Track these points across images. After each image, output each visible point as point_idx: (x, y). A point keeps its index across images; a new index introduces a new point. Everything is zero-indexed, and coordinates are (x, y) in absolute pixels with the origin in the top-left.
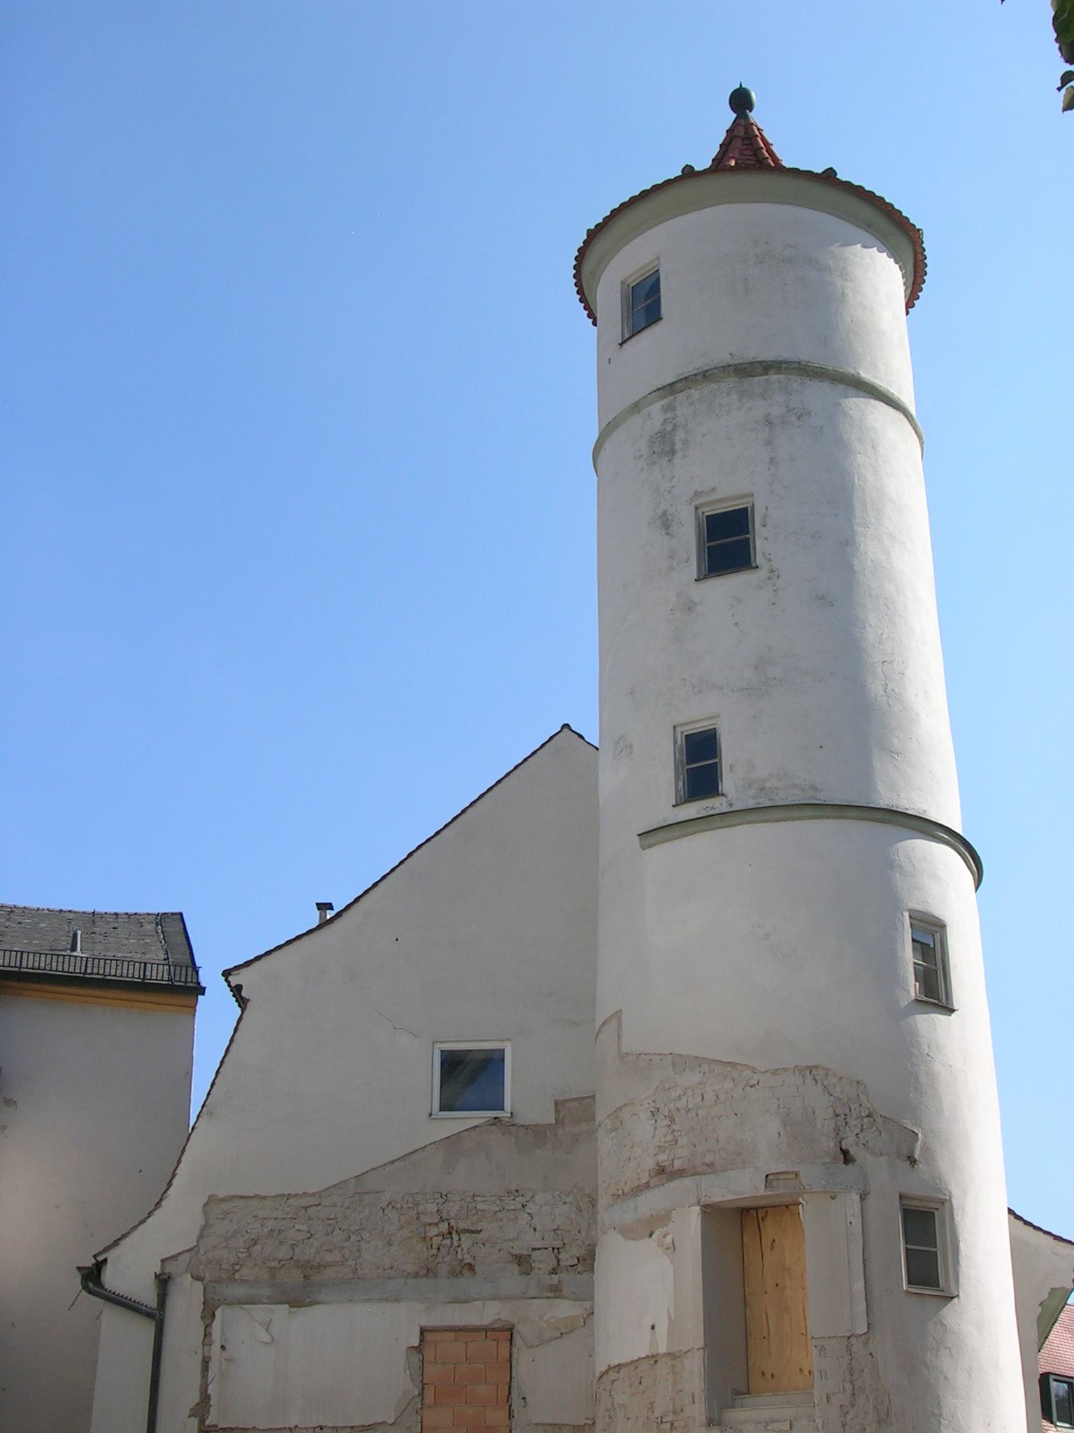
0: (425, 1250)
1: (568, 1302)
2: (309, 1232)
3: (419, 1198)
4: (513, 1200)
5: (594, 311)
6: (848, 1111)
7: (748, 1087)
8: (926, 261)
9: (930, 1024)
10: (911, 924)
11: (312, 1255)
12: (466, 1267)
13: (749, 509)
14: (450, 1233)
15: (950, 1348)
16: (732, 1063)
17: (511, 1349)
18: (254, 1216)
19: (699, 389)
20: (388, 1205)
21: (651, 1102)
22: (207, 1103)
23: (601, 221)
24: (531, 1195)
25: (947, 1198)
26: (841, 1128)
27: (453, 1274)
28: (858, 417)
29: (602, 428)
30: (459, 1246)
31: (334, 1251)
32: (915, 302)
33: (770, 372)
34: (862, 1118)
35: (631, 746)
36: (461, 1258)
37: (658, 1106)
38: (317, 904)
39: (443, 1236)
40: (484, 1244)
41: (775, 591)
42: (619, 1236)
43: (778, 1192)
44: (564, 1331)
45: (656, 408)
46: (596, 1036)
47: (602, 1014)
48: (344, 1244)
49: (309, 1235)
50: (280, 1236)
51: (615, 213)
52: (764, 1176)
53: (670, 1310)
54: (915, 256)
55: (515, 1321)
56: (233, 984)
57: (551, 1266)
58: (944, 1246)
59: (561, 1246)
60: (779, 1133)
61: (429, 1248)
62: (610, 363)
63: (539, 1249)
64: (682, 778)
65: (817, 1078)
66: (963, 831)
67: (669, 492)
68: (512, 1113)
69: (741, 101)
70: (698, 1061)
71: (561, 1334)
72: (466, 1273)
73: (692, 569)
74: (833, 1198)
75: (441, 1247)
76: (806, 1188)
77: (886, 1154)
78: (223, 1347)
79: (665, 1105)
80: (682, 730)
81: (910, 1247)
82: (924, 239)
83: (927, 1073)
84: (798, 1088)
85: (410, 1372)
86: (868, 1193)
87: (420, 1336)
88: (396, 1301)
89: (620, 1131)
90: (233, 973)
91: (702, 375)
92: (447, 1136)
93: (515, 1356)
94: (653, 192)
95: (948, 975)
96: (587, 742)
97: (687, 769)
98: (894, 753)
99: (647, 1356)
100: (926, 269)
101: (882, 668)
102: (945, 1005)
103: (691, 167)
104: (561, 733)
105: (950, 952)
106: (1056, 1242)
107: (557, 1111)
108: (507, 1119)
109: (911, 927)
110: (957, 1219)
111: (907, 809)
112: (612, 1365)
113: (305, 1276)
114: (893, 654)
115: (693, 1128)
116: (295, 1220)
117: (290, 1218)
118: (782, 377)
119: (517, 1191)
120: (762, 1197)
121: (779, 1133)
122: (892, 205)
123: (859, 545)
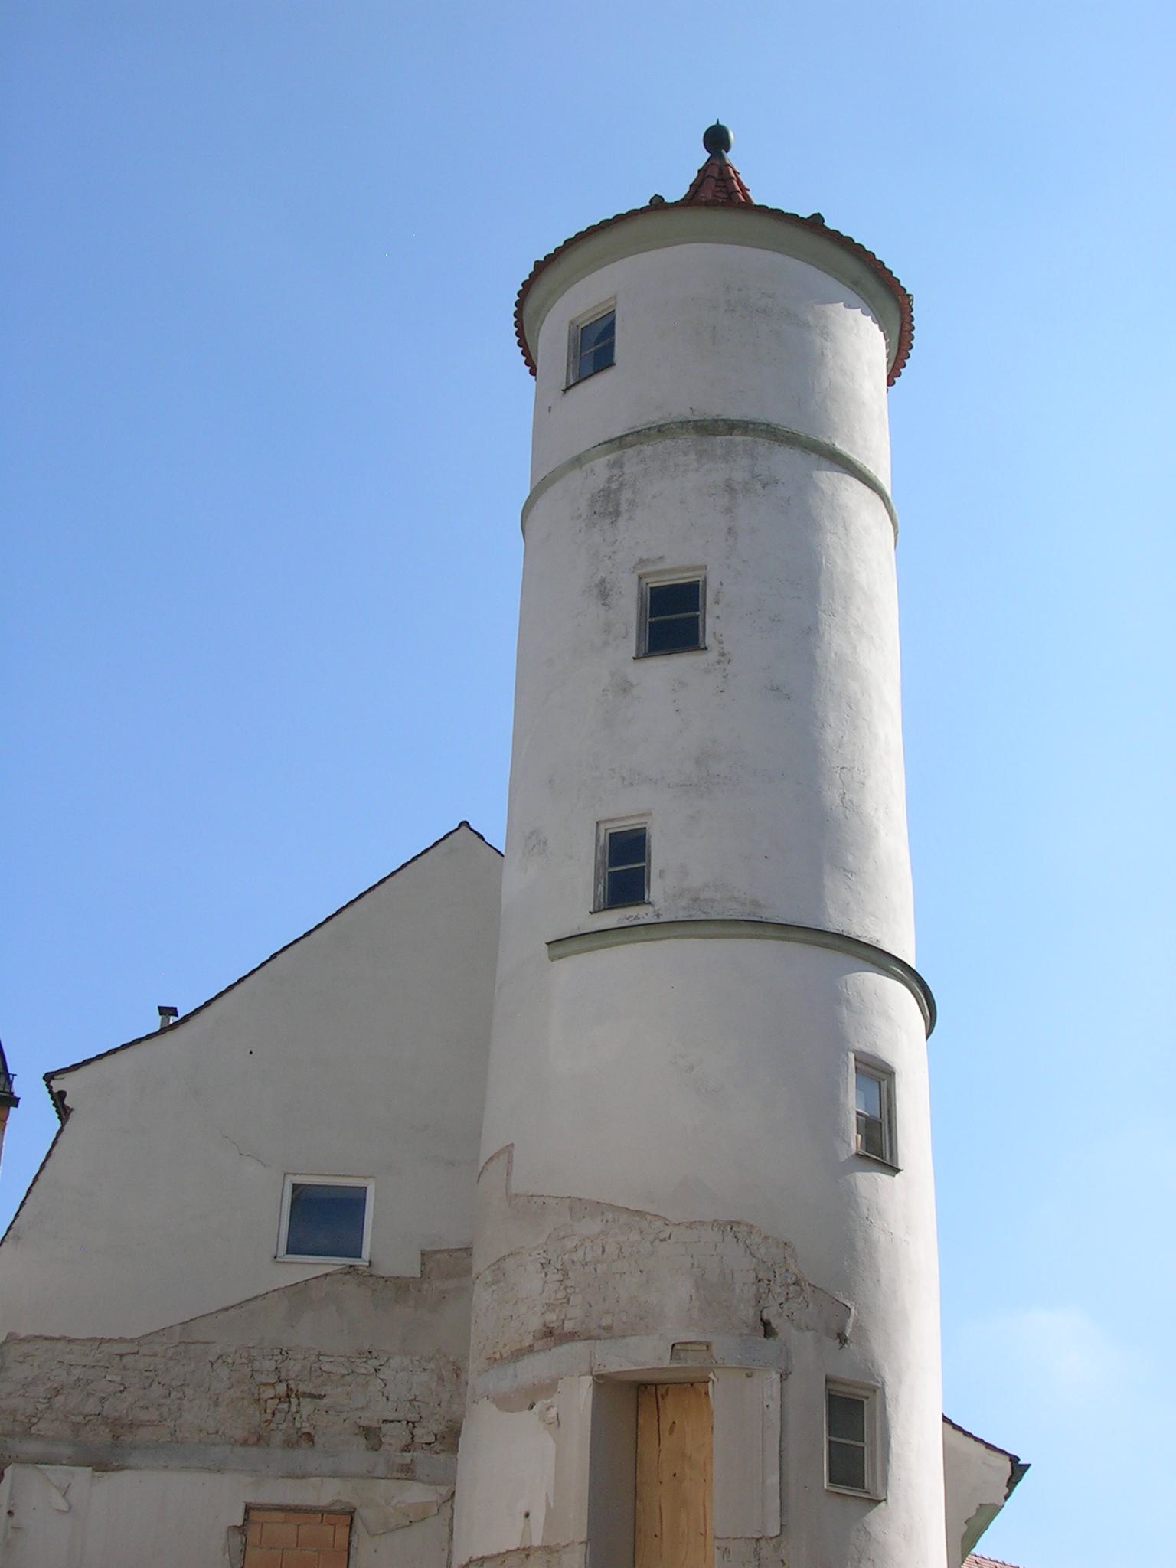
0: (257, 1413)
1: (421, 1485)
2: (122, 1384)
3: (254, 1353)
4: (365, 1362)
5: (533, 358)
6: (772, 1277)
7: (658, 1240)
8: (913, 332)
9: (871, 1182)
10: (856, 1068)
11: (125, 1411)
12: (303, 1437)
13: (701, 584)
14: (288, 1396)
15: (873, 1561)
16: (641, 1212)
17: (350, 1537)
18: (59, 1362)
19: (652, 445)
20: (218, 1358)
21: (542, 1251)
22: (14, 1226)
23: (561, 244)
24: (386, 1359)
25: (880, 1385)
26: (763, 1296)
27: (289, 1444)
28: (830, 493)
29: (536, 484)
30: (297, 1412)
31: (151, 1409)
32: (896, 379)
33: (735, 432)
34: (788, 1285)
35: (545, 843)
36: (299, 1426)
37: (549, 1258)
38: (160, 1008)
39: (280, 1399)
40: (327, 1412)
41: (724, 676)
42: (494, 1408)
43: (684, 1365)
44: (414, 1519)
45: (601, 464)
46: (479, 1176)
47: (488, 1148)
48: (164, 1401)
49: (122, 1388)
50: (88, 1388)
51: (569, 243)
52: (671, 1344)
53: (549, 1495)
54: (902, 325)
55: (357, 1504)
56: (55, 1090)
57: (404, 1443)
58: (873, 1443)
59: (417, 1420)
60: (691, 1296)
61: (263, 1411)
62: (549, 411)
63: (392, 1421)
64: (602, 881)
65: (739, 1236)
66: (916, 966)
67: (610, 558)
68: (370, 1262)
69: (716, 139)
70: (599, 1208)
71: (411, 1522)
72: (304, 1443)
73: (631, 645)
74: (748, 1376)
75: (276, 1412)
76: (718, 1362)
77: (813, 1329)
78: (10, 1513)
79: (558, 1256)
80: (607, 827)
81: (834, 1439)
82: (913, 306)
83: (865, 1240)
84: (716, 1246)
85: (229, 1555)
86: (790, 1373)
87: (245, 1514)
88: (219, 1471)
89: (502, 1284)
90: (55, 1077)
91: (656, 430)
92: (293, 1283)
93: (354, 1544)
94: (615, 223)
95: (894, 1129)
96: (488, 844)
97: (609, 873)
98: (848, 872)
99: (518, 1549)
100: (912, 342)
101: (840, 775)
102: (889, 1163)
103: (661, 197)
104: (459, 831)
105: (898, 1105)
106: (989, 1451)
107: (423, 1263)
108: (365, 1269)
109: (856, 1072)
110: (890, 1410)
111: (858, 936)
112: (474, 1558)
113: (113, 1436)
114: (854, 760)
115: (589, 1285)
116: (106, 1369)
117: (102, 1366)
118: (749, 438)
119: (370, 1352)
120: (666, 1369)
121: (691, 1296)
122: (883, 263)
123: (823, 634)
